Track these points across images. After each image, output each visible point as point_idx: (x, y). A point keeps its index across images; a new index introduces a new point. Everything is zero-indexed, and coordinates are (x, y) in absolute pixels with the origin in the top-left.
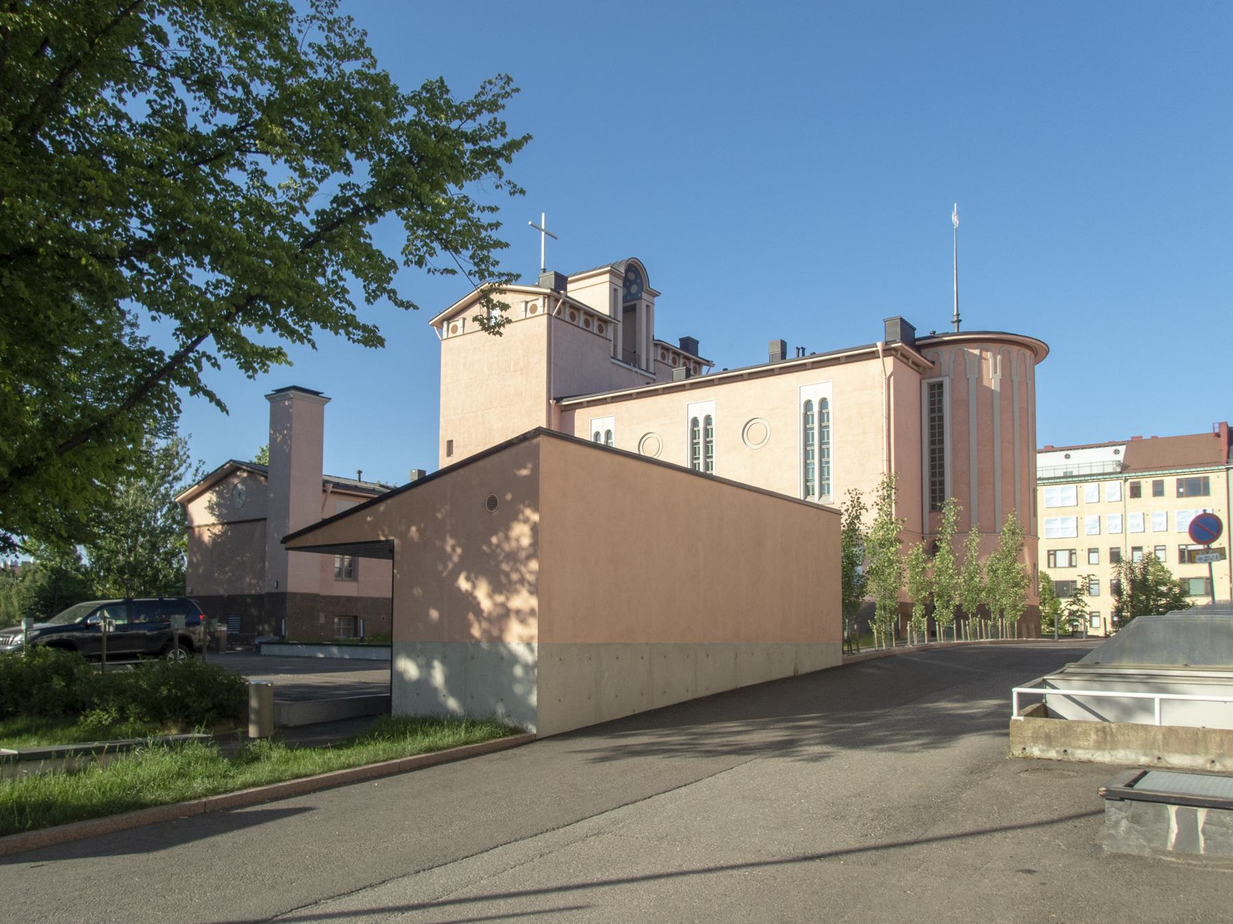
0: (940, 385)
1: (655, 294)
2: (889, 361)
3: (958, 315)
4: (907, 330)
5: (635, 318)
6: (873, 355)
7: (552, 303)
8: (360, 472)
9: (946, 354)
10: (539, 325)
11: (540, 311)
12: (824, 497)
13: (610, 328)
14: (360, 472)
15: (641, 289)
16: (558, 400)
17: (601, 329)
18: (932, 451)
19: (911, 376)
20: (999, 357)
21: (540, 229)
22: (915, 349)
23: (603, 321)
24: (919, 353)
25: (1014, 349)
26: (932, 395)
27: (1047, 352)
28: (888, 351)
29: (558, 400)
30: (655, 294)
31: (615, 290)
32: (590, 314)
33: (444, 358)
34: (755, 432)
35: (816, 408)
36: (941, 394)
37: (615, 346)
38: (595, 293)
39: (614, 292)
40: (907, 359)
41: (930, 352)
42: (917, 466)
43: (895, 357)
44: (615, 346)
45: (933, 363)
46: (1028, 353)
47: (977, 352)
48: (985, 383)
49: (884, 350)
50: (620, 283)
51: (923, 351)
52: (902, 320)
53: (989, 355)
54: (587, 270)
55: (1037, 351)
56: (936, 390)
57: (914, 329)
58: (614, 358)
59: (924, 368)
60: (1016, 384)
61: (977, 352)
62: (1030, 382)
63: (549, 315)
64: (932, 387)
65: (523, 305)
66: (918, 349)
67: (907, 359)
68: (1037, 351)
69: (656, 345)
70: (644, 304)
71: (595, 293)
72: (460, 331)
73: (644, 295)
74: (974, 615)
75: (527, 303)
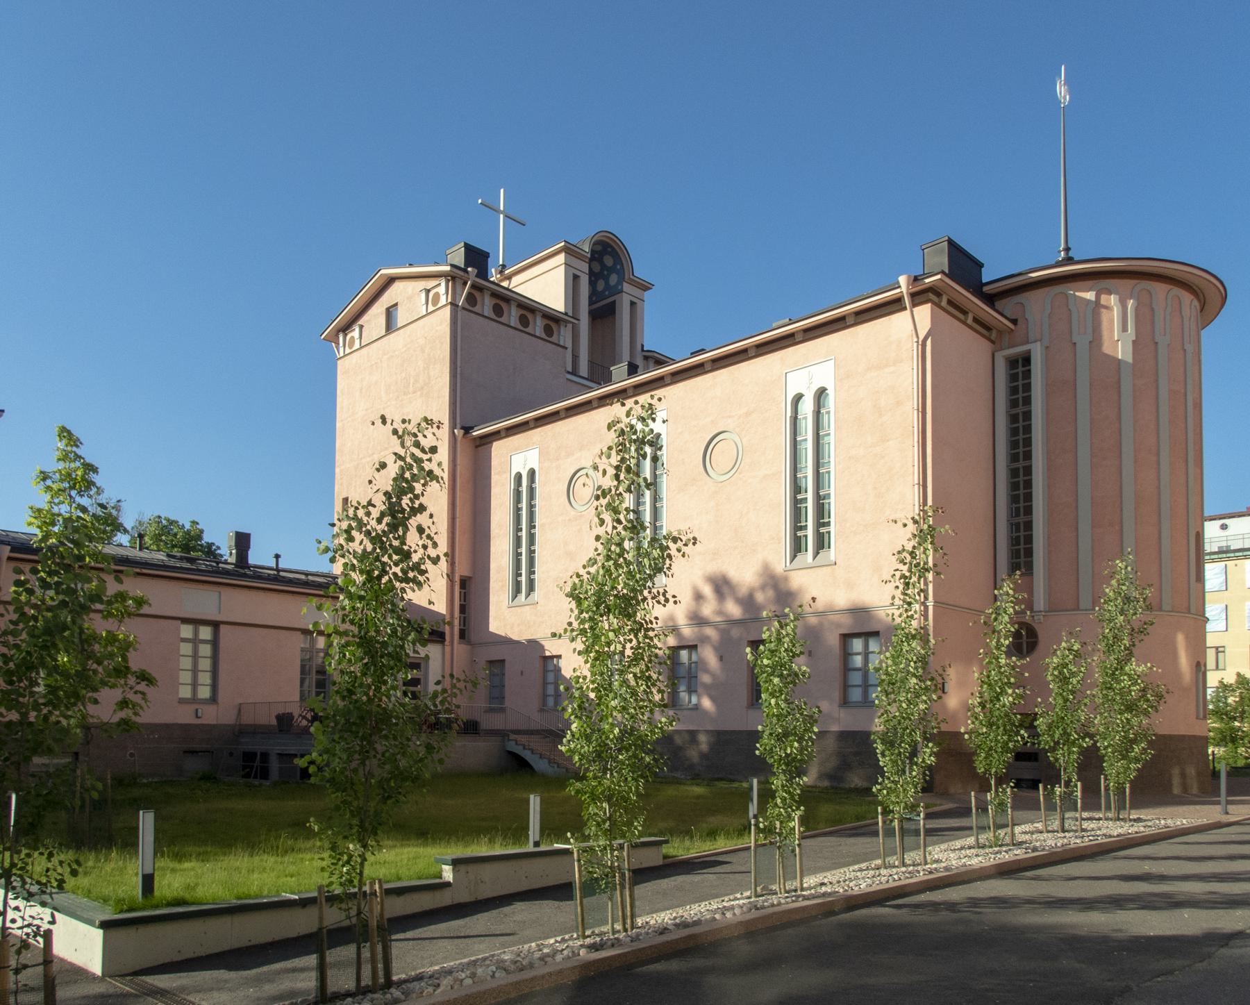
0: (1027, 360)
1: (645, 287)
2: (924, 313)
3: (1067, 249)
4: (963, 265)
5: (614, 323)
6: (894, 305)
7: (459, 286)
8: (277, 557)
9: (1036, 305)
10: (441, 321)
11: (443, 301)
12: (822, 553)
13: (565, 336)
14: (277, 557)
15: (622, 279)
16: (467, 430)
17: (549, 331)
18: (1014, 473)
19: (974, 347)
20: (1131, 303)
21: (498, 211)
22: (970, 291)
23: (552, 319)
24: (993, 307)
25: (1160, 289)
26: (1013, 378)
27: (1224, 299)
28: (918, 297)
29: (467, 430)
30: (645, 287)
31: (576, 277)
32: (529, 309)
33: (342, 383)
34: (722, 455)
35: (807, 407)
36: (1027, 374)
37: (575, 358)
38: (546, 284)
39: (573, 281)
40: (965, 313)
41: (1009, 305)
42: (981, 493)
43: (937, 305)
44: (575, 358)
45: (1014, 322)
46: (1186, 297)
47: (1090, 296)
48: (1107, 349)
49: (913, 295)
50: (585, 267)
51: (998, 304)
52: (951, 243)
53: (1113, 300)
54: (527, 252)
55: (1205, 294)
56: (1020, 367)
57: (981, 265)
58: (574, 372)
59: (1000, 332)
60: (1162, 350)
61: (1090, 296)
62: (1190, 348)
63: (453, 304)
64: (1013, 363)
65: (423, 295)
66: (990, 299)
67: (965, 313)
68: (1205, 294)
69: (646, 358)
70: (625, 301)
71: (546, 284)
72: (357, 345)
73: (626, 287)
74: (1000, 781)
75: (428, 291)
